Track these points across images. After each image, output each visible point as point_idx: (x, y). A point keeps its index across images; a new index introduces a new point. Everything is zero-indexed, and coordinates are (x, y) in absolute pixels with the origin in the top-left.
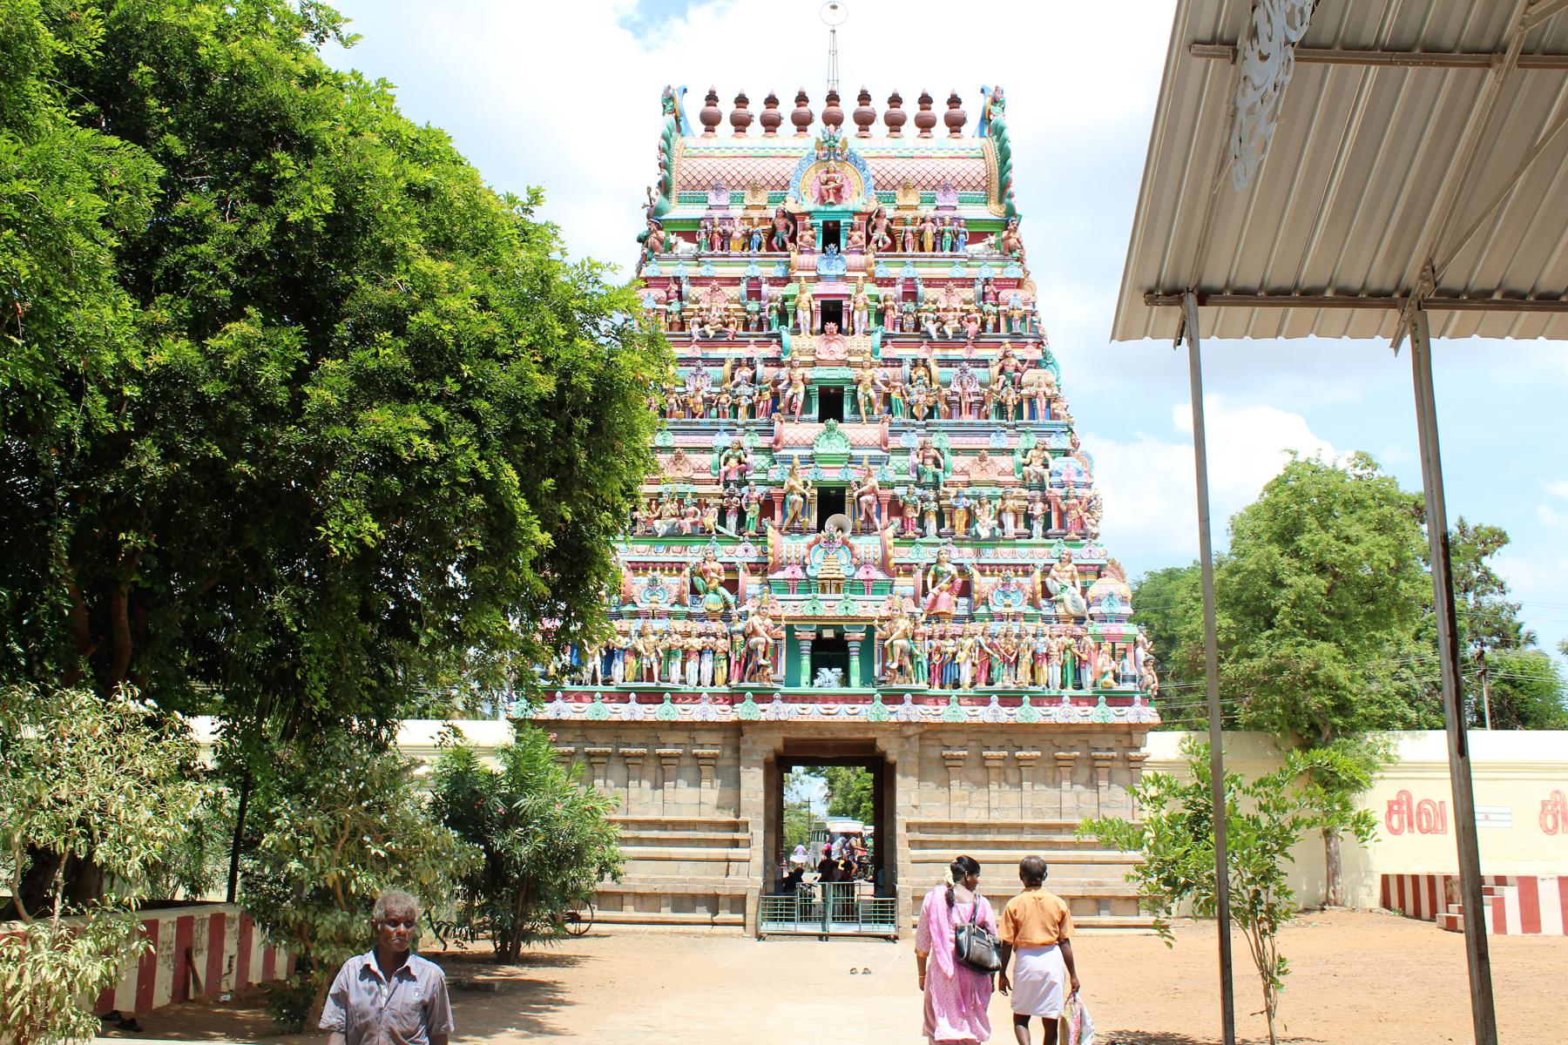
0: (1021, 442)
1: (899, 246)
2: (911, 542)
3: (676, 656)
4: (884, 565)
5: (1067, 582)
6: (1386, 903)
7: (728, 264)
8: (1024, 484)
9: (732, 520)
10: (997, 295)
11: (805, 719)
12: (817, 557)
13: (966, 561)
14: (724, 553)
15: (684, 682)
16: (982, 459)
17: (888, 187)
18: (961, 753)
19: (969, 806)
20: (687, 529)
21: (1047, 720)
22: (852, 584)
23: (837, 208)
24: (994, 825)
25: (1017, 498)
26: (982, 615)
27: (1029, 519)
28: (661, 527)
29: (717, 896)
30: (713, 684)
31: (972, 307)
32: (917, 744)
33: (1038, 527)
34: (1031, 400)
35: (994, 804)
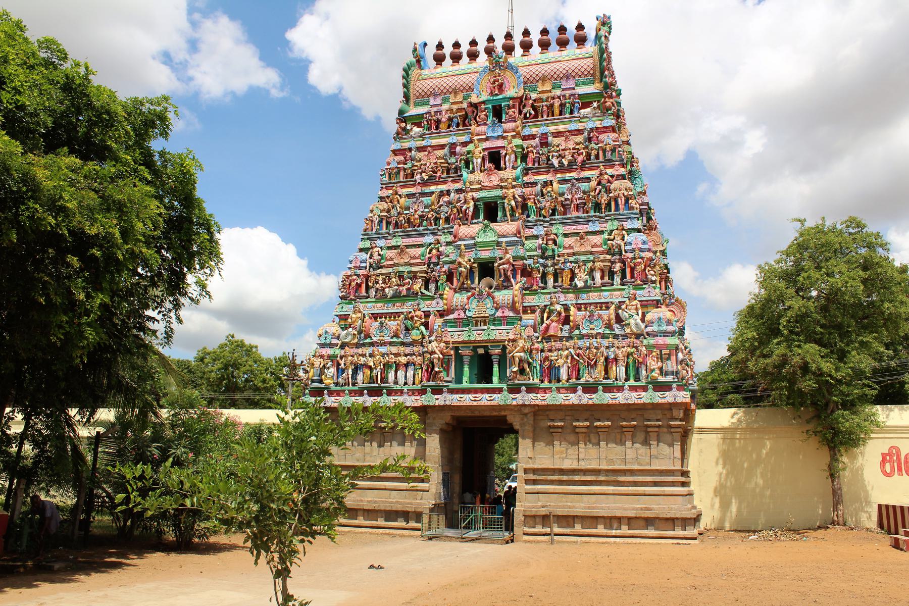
0: (608, 226)
1: (540, 115)
2: (535, 292)
3: (391, 368)
4: (513, 308)
5: (633, 312)
6: (881, 525)
7: (440, 137)
8: (609, 252)
9: (432, 286)
10: (598, 137)
11: (461, 404)
12: (473, 305)
13: (568, 303)
14: (425, 306)
15: (396, 383)
16: (582, 238)
17: (534, 81)
18: (559, 424)
19: (566, 457)
20: (404, 293)
21: (614, 402)
22: (494, 320)
23: (500, 97)
24: (581, 470)
25: (602, 261)
26: (576, 336)
27: (612, 274)
28: (389, 292)
29: (408, 512)
30: (414, 384)
31: (581, 146)
32: (532, 419)
33: (617, 279)
34: (616, 199)
35: (581, 456)
